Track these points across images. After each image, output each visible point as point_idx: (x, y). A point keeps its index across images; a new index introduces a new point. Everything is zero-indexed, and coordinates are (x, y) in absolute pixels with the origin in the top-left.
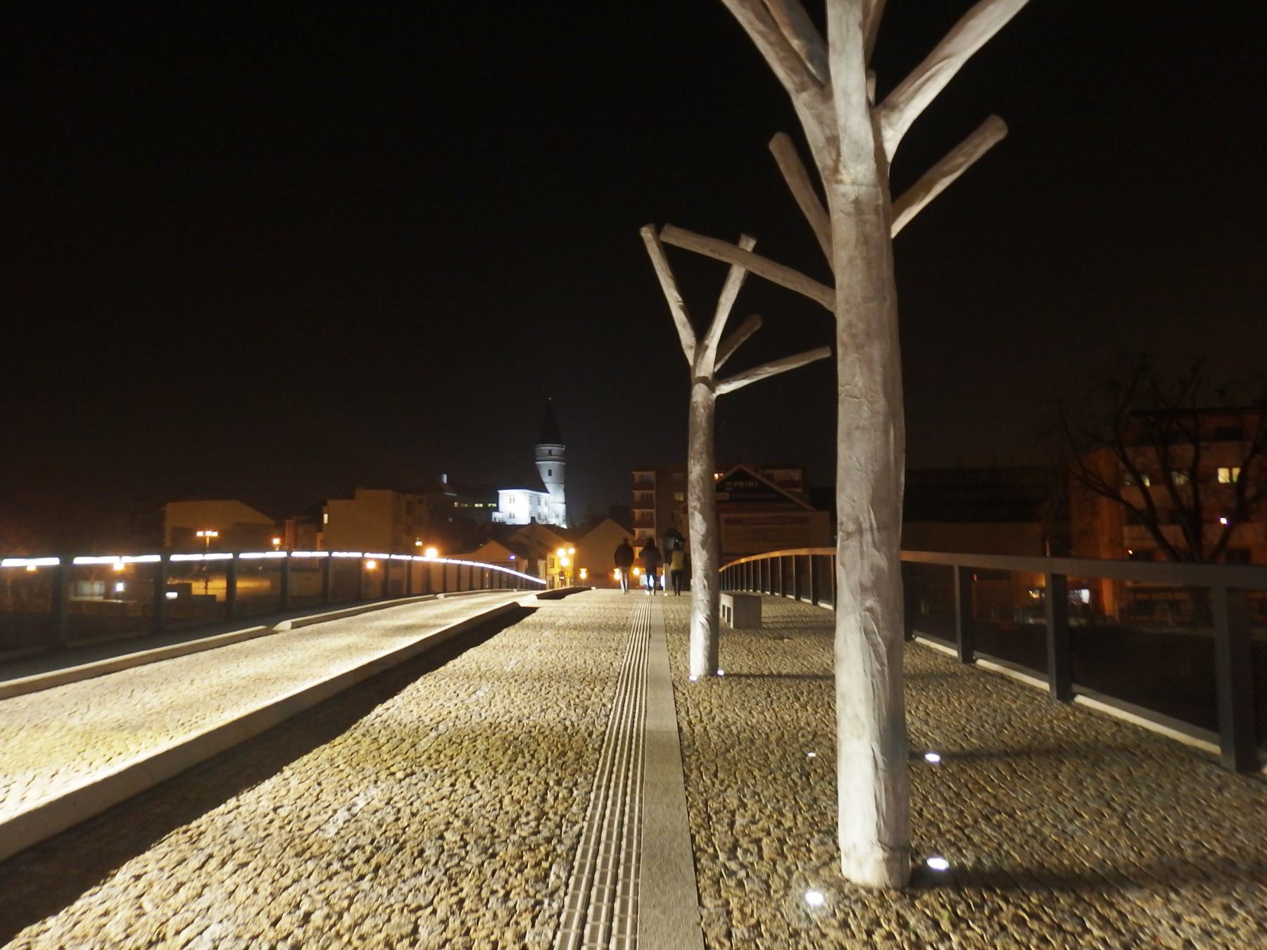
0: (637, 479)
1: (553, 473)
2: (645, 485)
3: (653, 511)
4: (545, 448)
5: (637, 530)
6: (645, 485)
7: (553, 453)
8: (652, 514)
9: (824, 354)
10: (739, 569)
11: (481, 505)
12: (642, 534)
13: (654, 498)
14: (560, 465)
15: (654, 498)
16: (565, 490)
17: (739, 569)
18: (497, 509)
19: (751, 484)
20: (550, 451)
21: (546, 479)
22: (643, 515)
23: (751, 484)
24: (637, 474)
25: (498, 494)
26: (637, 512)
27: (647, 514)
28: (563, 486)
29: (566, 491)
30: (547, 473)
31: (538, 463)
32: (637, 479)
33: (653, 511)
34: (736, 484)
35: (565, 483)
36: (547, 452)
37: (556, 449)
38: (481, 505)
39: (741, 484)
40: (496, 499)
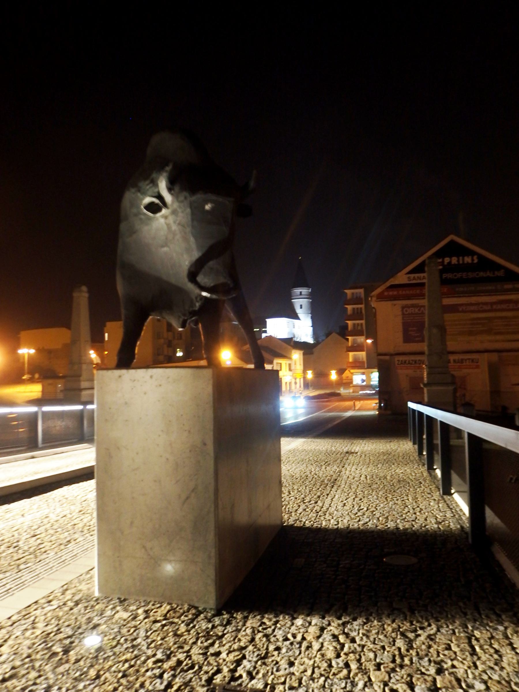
0: (349, 296)
1: (303, 307)
2: (356, 300)
3: (363, 322)
4: (297, 291)
5: (350, 338)
6: (356, 300)
7: (303, 293)
8: (362, 324)
9: (426, 399)
10: (450, 276)
11: (258, 330)
12: (354, 341)
13: (363, 311)
14: (308, 301)
15: (363, 311)
16: (312, 318)
17: (450, 276)
18: (265, 332)
19: (468, 260)
20: (301, 292)
21: (298, 311)
22: (354, 324)
23: (468, 260)
24: (349, 292)
25: (266, 321)
26: (350, 323)
27: (358, 324)
28: (310, 315)
29: (312, 318)
30: (299, 307)
31: (293, 300)
32: (349, 296)
33: (363, 322)
34: (447, 260)
35: (311, 313)
36: (299, 293)
37: (305, 291)
38: (258, 330)
39: (454, 260)
40: (264, 325)
